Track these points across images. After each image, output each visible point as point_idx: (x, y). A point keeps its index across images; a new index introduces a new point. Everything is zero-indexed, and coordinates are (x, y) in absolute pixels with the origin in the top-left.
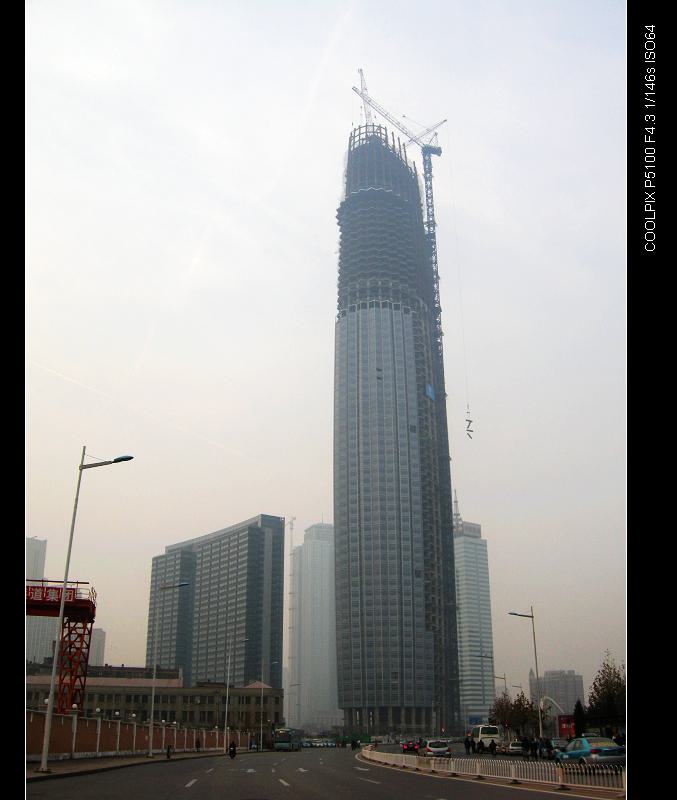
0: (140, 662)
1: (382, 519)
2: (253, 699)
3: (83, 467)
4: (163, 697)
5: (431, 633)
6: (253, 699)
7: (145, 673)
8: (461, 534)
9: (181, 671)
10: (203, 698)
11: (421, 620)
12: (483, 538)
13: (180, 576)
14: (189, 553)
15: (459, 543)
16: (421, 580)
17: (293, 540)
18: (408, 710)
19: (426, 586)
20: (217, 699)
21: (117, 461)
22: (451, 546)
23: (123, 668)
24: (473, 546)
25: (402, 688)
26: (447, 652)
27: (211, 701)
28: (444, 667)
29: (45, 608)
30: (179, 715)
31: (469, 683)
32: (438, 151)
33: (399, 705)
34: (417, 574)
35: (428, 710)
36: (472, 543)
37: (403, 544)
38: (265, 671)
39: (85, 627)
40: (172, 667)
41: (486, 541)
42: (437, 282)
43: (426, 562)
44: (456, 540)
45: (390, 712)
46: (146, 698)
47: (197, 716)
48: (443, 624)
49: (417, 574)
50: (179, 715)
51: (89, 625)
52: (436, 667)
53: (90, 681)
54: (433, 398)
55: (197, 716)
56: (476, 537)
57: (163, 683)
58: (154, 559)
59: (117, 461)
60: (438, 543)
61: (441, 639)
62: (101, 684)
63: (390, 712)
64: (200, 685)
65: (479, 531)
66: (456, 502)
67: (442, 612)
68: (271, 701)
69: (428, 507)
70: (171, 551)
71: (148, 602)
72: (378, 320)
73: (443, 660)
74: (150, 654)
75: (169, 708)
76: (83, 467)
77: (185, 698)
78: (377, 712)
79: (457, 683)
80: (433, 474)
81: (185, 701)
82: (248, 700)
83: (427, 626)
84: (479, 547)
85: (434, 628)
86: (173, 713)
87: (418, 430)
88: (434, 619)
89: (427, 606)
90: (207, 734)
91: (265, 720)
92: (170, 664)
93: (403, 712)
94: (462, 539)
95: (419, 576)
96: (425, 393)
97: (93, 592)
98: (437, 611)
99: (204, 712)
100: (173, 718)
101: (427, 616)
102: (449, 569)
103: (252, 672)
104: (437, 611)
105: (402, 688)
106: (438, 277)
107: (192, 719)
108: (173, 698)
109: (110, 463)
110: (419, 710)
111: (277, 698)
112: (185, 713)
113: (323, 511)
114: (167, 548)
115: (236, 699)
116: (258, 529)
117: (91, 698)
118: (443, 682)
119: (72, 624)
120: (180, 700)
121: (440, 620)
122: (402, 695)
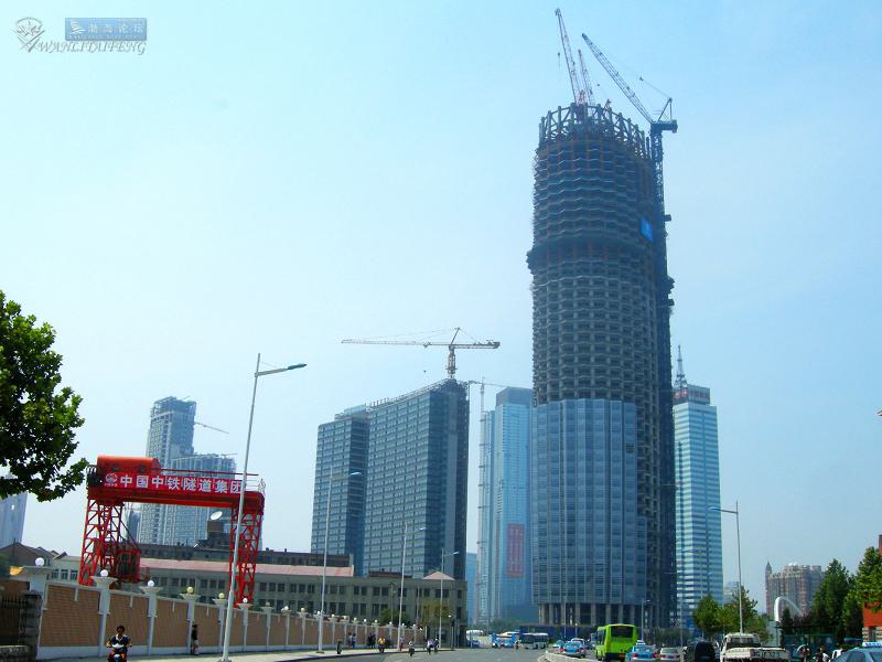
0: (304, 545)
1: (588, 508)
2: (432, 593)
3: (258, 374)
4: (335, 587)
6: (432, 593)
7: (313, 559)
8: (682, 400)
9: (351, 556)
10: (376, 591)
11: (633, 503)
13: (352, 444)
14: (363, 425)
15: (681, 412)
16: (633, 456)
17: (480, 405)
20: (392, 591)
21: (291, 368)
23: (285, 553)
24: (700, 414)
25: (608, 570)
26: (662, 540)
27: (385, 592)
28: (659, 525)
30: (349, 607)
32: (673, 127)
34: (629, 449)
35: (638, 608)
36: (699, 411)
37: (613, 550)
38: (448, 554)
39: (254, 519)
40: (342, 552)
43: (639, 435)
44: (675, 408)
45: (593, 609)
47: (369, 609)
49: (629, 449)
50: (349, 607)
51: (258, 517)
52: (648, 559)
53: (261, 568)
55: (369, 609)
56: (704, 403)
57: (332, 571)
58: (320, 427)
59: (291, 368)
60: (654, 402)
61: (655, 526)
63: (593, 609)
64: (373, 574)
66: (680, 360)
67: (659, 492)
68: (453, 594)
70: (341, 418)
71: (316, 444)
72: (589, 417)
73: (658, 551)
75: (337, 599)
76: (258, 374)
77: (356, 591)
78: (578, 609)
79: (674, 578)
81: (356, 592)
82: (427, 592)
83: (639, 511)
84: (706, 415)
86: (342, 605)
87: (636, 450)
89: (639, 487)
91: (445, 617)
92: (338, 548)
93: (608, 609)
94: (685, 405)
95: (630, 452)
97: (262, 484)
98: (652, 490)
99: (377, 606)
100: (342, 612)
101: (639, 499)
102: (668, 443)
103: (432, 562)
104: (652, 490)
105: (608, 570)
107: (363, 612)
111: (460, 592)
112: (355, 605)
113: (518, 368)
115: (414, 591)
118: (658, 576)
120: (350, 591)
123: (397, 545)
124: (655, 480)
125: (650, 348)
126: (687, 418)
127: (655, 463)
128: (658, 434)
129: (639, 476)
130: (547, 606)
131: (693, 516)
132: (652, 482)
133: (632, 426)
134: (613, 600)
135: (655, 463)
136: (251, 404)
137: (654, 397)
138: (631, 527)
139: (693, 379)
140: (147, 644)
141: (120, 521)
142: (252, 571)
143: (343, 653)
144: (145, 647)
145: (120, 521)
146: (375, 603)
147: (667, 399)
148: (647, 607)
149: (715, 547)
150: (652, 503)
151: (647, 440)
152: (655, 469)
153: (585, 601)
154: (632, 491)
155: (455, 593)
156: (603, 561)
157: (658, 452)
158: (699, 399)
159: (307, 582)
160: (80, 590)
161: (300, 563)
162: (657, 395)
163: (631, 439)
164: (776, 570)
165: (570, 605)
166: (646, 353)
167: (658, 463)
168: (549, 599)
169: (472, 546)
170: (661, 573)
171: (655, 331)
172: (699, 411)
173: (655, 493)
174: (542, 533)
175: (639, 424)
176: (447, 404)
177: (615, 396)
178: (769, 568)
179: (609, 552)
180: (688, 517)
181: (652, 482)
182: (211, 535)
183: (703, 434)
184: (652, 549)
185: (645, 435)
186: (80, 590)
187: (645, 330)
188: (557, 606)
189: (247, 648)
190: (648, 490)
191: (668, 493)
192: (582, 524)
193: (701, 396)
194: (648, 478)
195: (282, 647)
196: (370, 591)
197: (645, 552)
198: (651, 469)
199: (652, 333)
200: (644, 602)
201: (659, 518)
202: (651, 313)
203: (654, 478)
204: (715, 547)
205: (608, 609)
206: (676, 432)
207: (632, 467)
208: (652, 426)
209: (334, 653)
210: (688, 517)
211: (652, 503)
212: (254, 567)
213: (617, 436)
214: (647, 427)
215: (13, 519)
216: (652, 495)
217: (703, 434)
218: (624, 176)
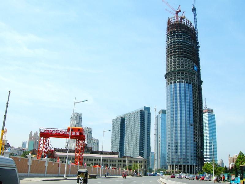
1: (181, 143)
3: (75, 103)
5: (196, 143)
7: (112, 153)
8: (206, 112)
11: (192, 139)
12: (214, 113)
15: (205, 116)
16: (192, 127)
18: (188, 166)
19: (194, 129)
21: (83, 101)
22: (202, 116)
24: (211, 116)
25: (186, 156)
26: (200, 146)
29: (76, 134)
31: (209, 161)
33: (185, 164)
34: (191, 125)
36: (211, 115)
41: (215, 114)
42: (197, 34)
43: (194, 121)
44: (204, 114)
45: (182, 166)
46: (100, 160)
48: (199, 140)
52: (197, 153)
54: (196, 70)
59: (83, 101)
60: (198, 112)
61: (198, 145)
62: (95, 156)
63: (182, 166)
65: (213, 111)
67: (199, 136)
69: (195, 104)
74: (112, 148)
75: (114, 163)
76: (75, 103)
78: (178, 166)
79: (203, 158)
80: (196, 94)
83: (194, 141)
84: (212, 116)
85: (196, 141)
88: (196, 138)
89: (194, 135)
90: (93, 169)
93: (186, 166)
94: (207, 113)
96: (194, 69)
99: (119, 165)
101: (194, 138)
105: (186, 156)
106: (197, 32)
108: (107, 160)
109: (81, 102)
110: (191, 166)
112: (119, 165)
114: (117, 116)
116: (144, 111)
117: (85, 159)
119: (79, 141)
120: (117, 161)
121: (198, 139)
122: (186, 158)
123: (132, 149)
124: (198, 133)
125: (196, 99)
126: (208, 120)
127: (198, 128)
128: (199, 121)
129: (194, 132)
130: (170, 165)
131: (209, 142)
132: (197, 133)
133: (192, 119)
134: (187, 164)
135: (198, 128)
136: (73, 111)
137: (198, 111)
138: (192, 145)
139: (209, 107)
140: (45, 173)
141: (49, 142)
142: (82, 155)
143: (107, 177)
144: (27, 174)
145: (49, 142)
146: (119, 163)
147: (201, 112)
148: (196, 166)
149: (215, 152)
150: (197, 139)
151: (196, 122)
152: (198, 130)
153: (180, 164)
154: (192, 136)
155: (144, 162)
156: (185, 154)
157: (199, 125)
158: (210, 112)
159: (106, 159)
160: (21, 159)
161: (106, 154)
162: (199, 111)
163: (192, 122)
164: (231, 156)
165: (176, 165)
166: (196, 100)
167: (199, 128)
168: (171, 164)
169: (153, 150)
170: (200, 157)
171: (198, 94)
172: (211, 115)
173: (198, 136)
174: (169, 146)
175: (194, 118)
176: (144, 115)
177: (187, 83)
178: (229, 156)
179: (186, 151)
180: (208, 148)
181: (197, 133)
182: (84, 147)
183: (212, 127)
184: (198, 151)
185: (195, 121)
186: (21, 159)
187: (194, 77)
188: (173, 165)
189: (46, 175)
190: (196, 135)
191: (202, 136)
192: (179, 144)
193: (211, 111)
194: (196, 132)
195: (57, 175)
196: (122, 161)
197: (196, 155)
198: (197, 130)
199: (196, 80)
200: (195, 164)
201: (199, 143)
202: (198, 106)
203: (198, 132)
204: (215, 152)
205: (186, 166)
206: (204, 121)
207: (192, 130)
208: (197, 119)
209: (105, 177)
210: (208, 148)
211: (197, 139)
212: (83, 154)
213: (188, 121)
214: (196, 119)
215: (37, 143)
216: (197, 137)
217: (212, 127)
218: (189, 52)
